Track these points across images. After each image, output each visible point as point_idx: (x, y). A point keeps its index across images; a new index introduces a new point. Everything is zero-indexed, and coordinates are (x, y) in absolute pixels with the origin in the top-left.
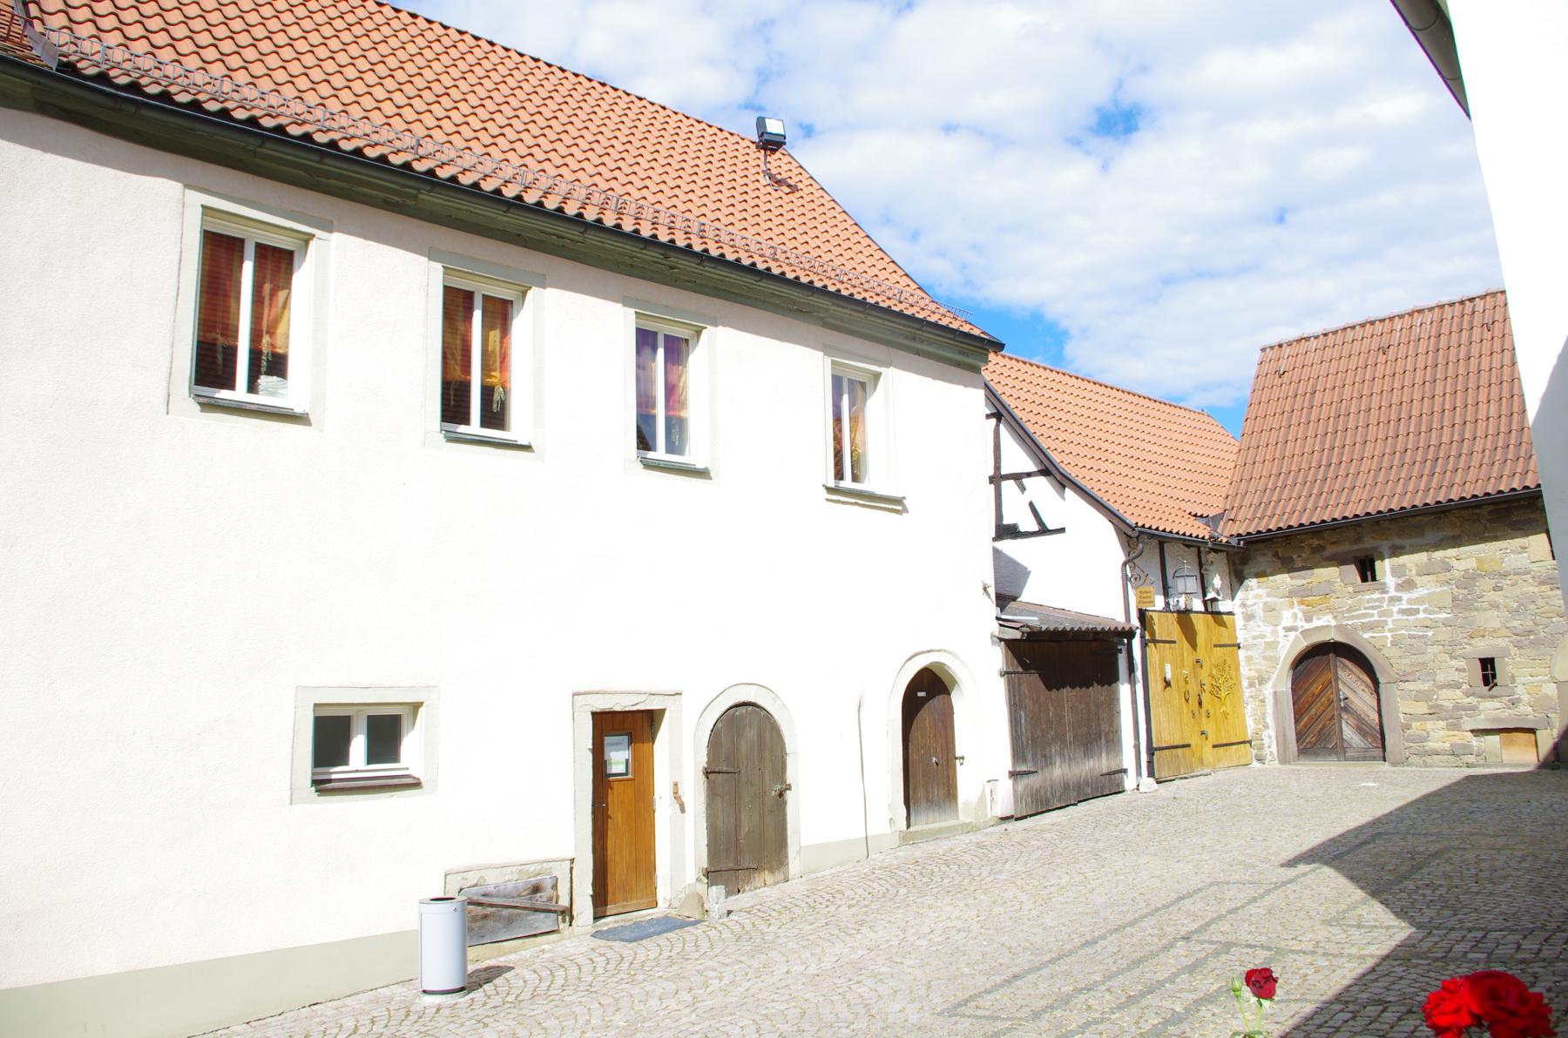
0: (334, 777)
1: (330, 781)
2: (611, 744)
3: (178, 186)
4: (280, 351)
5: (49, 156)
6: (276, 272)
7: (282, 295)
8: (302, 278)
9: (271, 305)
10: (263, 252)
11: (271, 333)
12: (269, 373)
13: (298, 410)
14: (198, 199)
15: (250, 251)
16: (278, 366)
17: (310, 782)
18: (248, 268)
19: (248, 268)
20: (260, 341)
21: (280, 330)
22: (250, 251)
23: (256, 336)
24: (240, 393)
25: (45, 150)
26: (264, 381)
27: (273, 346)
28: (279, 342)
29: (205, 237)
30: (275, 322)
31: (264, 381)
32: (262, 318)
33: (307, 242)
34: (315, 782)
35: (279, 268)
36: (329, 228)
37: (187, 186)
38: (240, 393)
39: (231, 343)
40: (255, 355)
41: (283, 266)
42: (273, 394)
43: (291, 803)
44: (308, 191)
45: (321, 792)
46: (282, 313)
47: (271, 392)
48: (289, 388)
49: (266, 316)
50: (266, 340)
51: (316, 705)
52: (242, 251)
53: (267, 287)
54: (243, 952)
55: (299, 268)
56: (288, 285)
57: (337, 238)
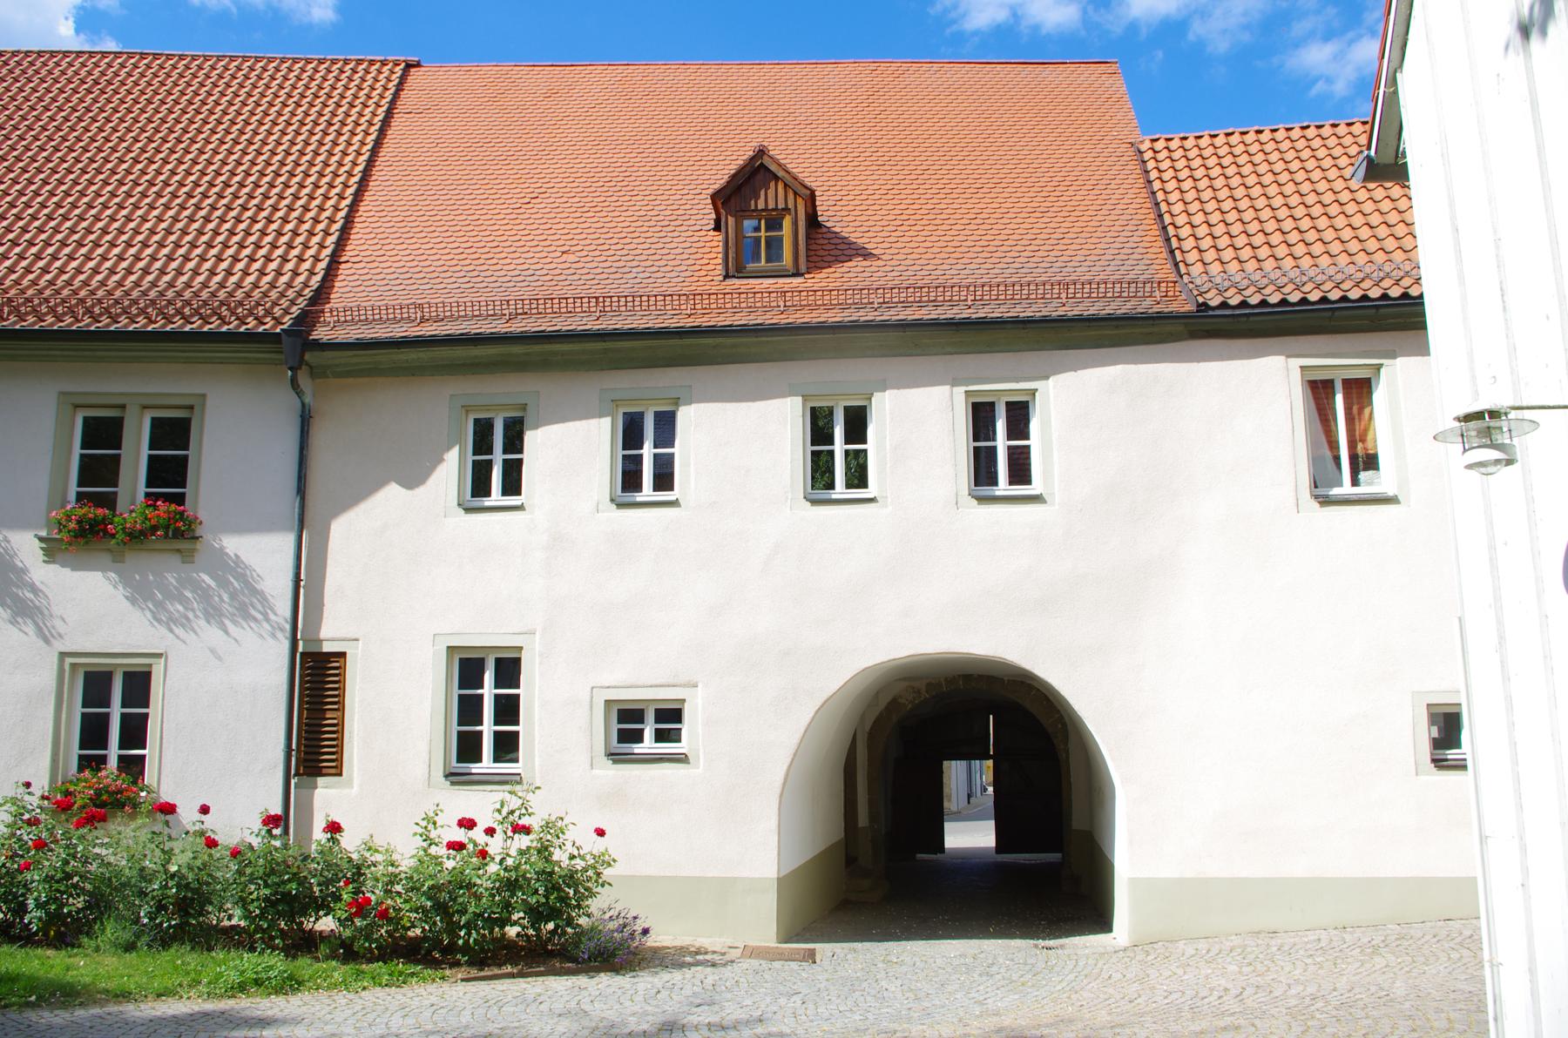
0: (1449, 757)
1: (1447, 760)
2: (725, 888)
3: (1282, 358)
4: (1371, 452)
5: (1202, 364)
6: (1360, 396)
7: (1367, 411)
8: (1379, 396)
9: (1360, 420)
10: (1348, 384)
11: (1363, 441)
12: (1365, 469)
13: (1391, 494)
14: (1296, 363)
15: (1339, 386)
16: (1371, 462)
17: (1429, 761)
18: (1339, 399)
19: (1339, 399)
20: (1356, 447)
21: (1370, 437)
22: (1339, 386)
23: (1352, 445)
24: (1346, 489)
25: (1199, 362)
26: (1363, 476)
27: (1366, 449)
28: (1370, 444)
29: (1306, 384)
30: (1366, 431)
31: (1363, 476)
32: (1355, 430)
33: (1379, 370)
34: (1434, 761)
35: (1362, 393)
36: (1392, 355)
37: (1288, 356)
38: (1346, 489)
39: (665, 471)
40: (1353, 458)
41: (1365, 390)
42: (1370, 484)
43: (1417, 774)
44: (1334, 336)
45: (1440, 768)
46: (1369, 424)
47: (1371, 483)
48: (204, 521)
49: (1357, 427)
50: (1360, 446)
51: (1428, 705)
52: (1333, 388)
53: (1355, 408)
54: (1390, 875)
55: (1377, 388)
56: (1370, 403)
57: (1401, 361)
